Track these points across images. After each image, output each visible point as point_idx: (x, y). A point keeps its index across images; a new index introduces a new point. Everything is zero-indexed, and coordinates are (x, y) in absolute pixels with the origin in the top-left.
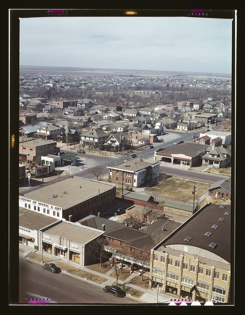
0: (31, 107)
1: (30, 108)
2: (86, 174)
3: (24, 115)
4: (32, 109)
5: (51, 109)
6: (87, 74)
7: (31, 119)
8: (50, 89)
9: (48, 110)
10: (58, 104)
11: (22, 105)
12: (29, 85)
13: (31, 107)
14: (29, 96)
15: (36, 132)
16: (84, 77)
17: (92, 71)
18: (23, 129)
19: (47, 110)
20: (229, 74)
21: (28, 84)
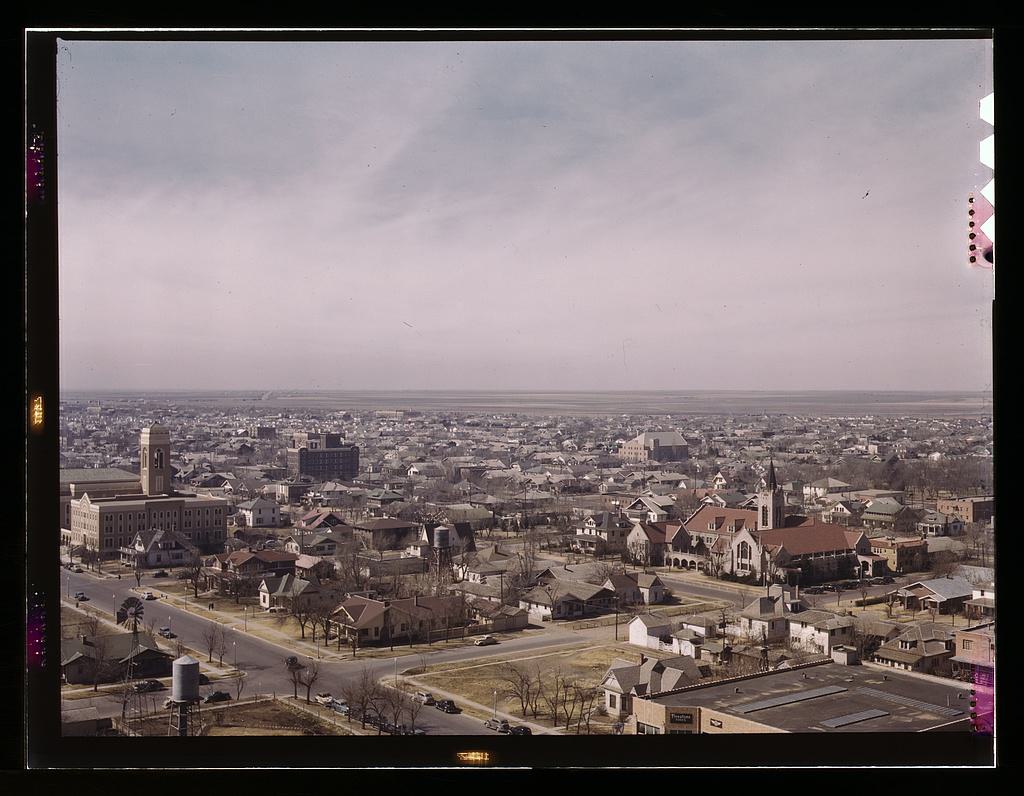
0: (882, 517)
1: (871, 521)
2: (542, 604)
3: (893, 544)
4: (880, 523)
5: (946, 525)
6: (513, 401)
7: (913, 555)
8: (883, 460)
9: (937, 528)
10: (956, 508)
11: (846, 510)
12: (801, 451)
13: (882, 517)
14: (843, 484)
15: (969, 597)
16: (951, 422)
17: (956, 401)
18: (921, 586)
19: (931, 530)
20: (974, 395)
21: (798, 445)
